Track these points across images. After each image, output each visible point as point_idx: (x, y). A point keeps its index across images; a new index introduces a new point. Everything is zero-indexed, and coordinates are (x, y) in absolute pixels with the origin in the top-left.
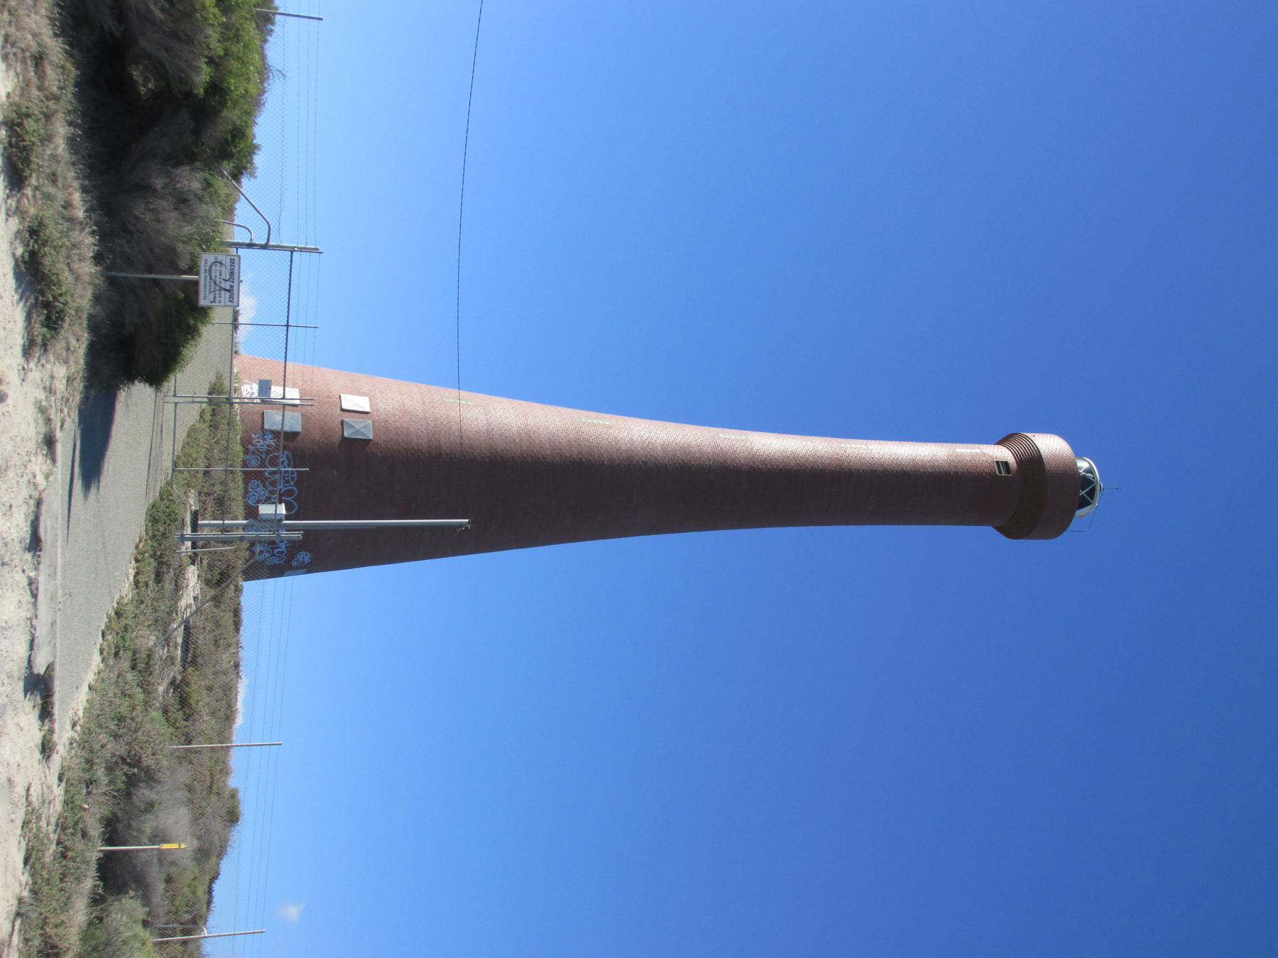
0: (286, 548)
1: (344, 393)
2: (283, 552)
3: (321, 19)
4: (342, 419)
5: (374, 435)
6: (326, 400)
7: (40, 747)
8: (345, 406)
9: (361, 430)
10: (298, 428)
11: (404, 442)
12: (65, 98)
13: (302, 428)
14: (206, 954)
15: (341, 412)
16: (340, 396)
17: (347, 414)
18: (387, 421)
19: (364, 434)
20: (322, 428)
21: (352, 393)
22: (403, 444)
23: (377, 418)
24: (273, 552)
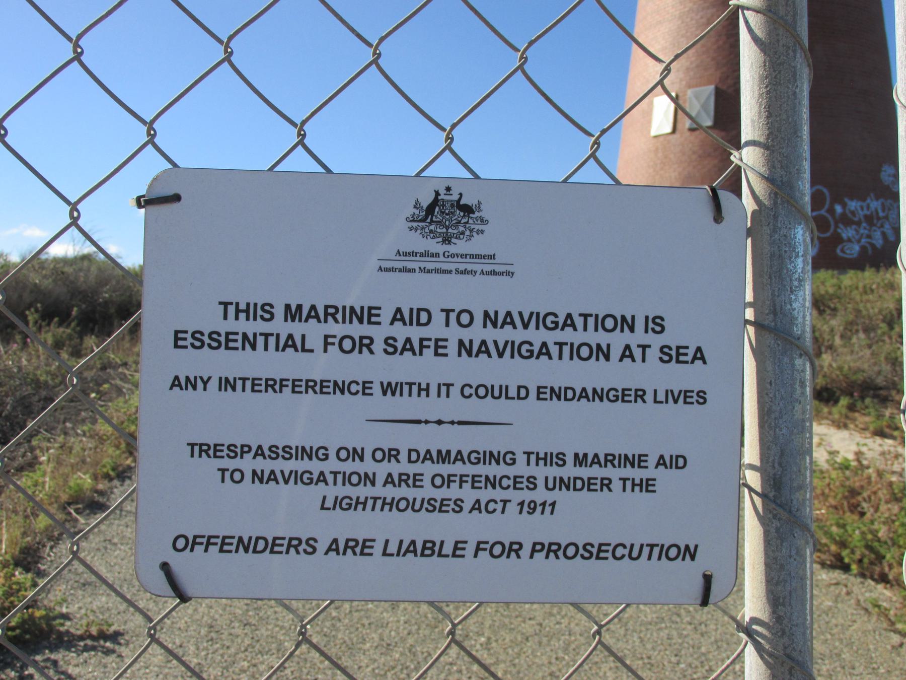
0: (877, 199)
1: (649, 132)
2: (883, 205)
3: (177, 198)
4: (686, 130)
5: (705, 85)
6: (660, 155)
7: (188, 663)
8: (669, 129)
9: (702, 101)
10: (711, 88)
11: (717, 41)
12: (391, 619)
13: (709, 83)
14: (858, 577)
15: (677, 132)
16: (656, 137)
17: (679, 126)
18: (687, 69)
19: (708, 98)
20: (700, 157)
21: (649, 122)
22: (721, 43)
23: (684, 83)
24: (884, 217)
